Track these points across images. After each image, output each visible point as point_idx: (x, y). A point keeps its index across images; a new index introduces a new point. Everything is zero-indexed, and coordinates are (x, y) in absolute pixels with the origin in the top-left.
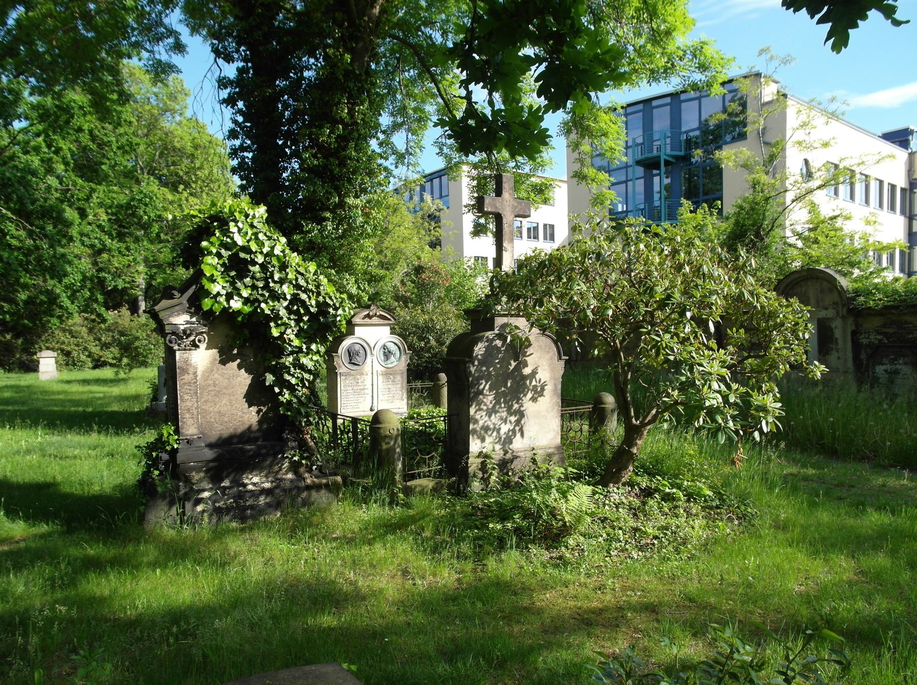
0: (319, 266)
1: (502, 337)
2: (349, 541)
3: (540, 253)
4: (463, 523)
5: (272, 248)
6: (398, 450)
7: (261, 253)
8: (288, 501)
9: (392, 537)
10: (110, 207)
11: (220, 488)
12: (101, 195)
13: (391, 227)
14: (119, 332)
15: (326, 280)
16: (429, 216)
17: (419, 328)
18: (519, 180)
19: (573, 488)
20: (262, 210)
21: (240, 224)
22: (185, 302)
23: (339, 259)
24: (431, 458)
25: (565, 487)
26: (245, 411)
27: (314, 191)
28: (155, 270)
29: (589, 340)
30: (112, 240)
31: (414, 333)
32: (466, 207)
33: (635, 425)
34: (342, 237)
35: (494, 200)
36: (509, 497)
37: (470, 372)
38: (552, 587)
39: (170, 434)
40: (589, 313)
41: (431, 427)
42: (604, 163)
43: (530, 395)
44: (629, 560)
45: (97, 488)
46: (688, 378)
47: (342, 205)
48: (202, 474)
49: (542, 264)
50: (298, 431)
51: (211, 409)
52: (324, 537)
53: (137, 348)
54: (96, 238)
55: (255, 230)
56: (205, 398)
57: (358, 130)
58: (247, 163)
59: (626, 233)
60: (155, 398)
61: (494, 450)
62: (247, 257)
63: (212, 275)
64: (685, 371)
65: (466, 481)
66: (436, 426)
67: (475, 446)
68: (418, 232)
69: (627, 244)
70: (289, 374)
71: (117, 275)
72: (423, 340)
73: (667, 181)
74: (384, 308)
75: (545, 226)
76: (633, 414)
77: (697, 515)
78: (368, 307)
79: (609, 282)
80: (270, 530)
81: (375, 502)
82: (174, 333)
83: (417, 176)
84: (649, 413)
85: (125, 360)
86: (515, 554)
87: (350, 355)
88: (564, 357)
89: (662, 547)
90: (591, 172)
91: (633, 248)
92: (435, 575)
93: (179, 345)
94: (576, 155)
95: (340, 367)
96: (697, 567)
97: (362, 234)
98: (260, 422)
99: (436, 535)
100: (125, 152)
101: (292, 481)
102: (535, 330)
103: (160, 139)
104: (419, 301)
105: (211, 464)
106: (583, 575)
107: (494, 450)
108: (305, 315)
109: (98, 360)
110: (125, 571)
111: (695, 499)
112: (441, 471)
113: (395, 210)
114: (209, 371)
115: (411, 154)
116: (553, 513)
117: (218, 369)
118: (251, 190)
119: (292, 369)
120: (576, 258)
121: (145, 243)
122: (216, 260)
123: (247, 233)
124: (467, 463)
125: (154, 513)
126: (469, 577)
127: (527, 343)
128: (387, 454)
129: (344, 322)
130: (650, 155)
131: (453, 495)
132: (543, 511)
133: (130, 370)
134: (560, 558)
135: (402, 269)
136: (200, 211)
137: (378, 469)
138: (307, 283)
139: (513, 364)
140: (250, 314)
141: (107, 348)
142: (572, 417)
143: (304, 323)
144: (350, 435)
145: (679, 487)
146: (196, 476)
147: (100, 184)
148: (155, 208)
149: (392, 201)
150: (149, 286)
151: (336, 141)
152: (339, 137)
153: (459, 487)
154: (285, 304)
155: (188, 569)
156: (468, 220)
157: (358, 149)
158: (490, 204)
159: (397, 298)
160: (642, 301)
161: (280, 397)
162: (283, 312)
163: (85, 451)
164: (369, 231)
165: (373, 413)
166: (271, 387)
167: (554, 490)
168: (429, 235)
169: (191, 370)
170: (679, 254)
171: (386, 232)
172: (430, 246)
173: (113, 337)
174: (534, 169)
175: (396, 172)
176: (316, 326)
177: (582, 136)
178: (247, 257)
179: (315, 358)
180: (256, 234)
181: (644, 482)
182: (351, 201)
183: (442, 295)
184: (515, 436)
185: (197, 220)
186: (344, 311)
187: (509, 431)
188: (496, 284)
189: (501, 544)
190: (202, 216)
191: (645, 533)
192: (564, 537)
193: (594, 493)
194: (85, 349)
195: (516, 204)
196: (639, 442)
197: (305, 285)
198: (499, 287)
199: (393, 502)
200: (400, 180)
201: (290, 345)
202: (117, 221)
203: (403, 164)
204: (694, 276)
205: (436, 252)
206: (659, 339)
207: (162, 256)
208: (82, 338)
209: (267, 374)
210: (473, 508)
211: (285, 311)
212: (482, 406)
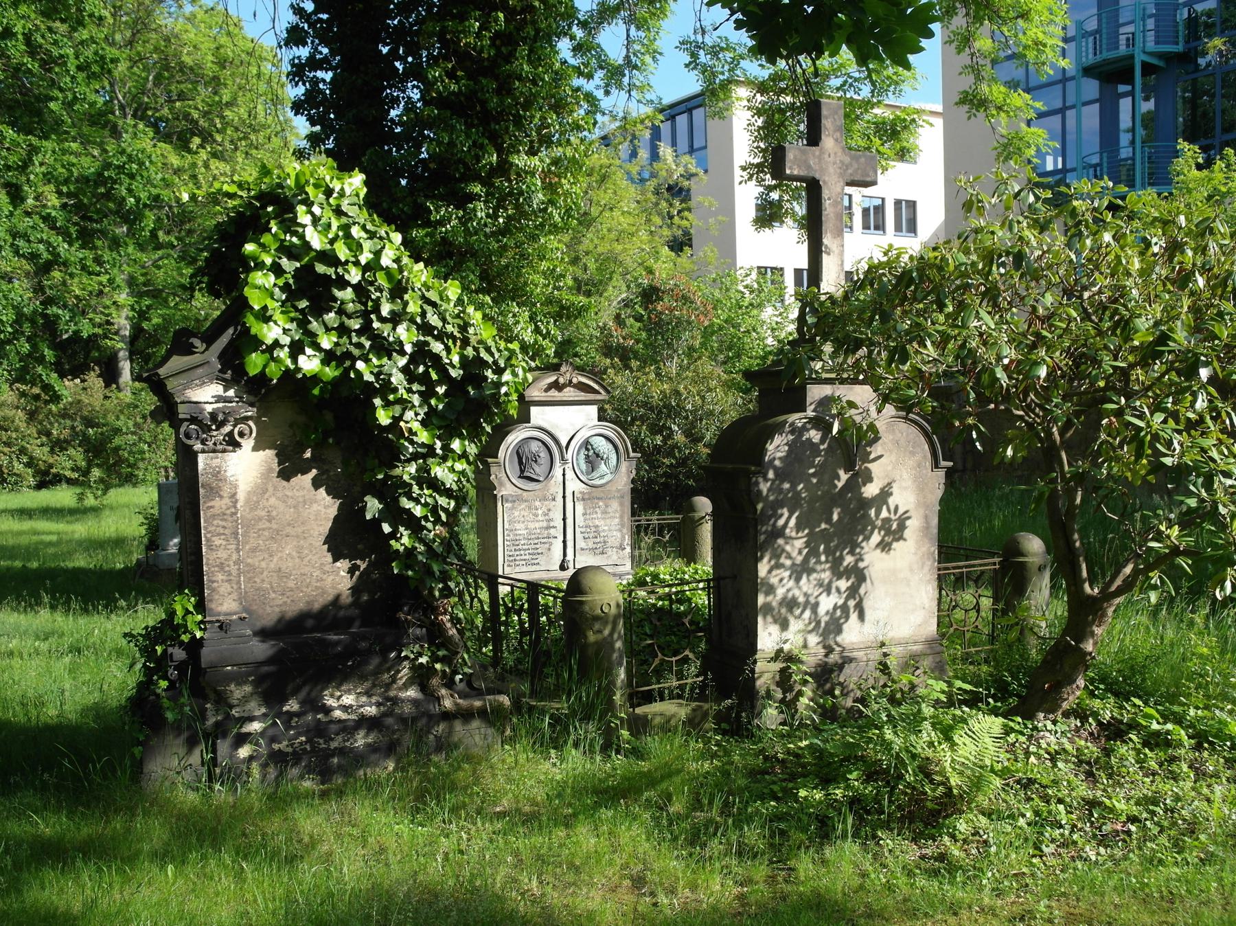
0: (465, 288)
1: (821, 423)
2: (529, 819)
3: (898, 256)
4: (747, 788)
5: (378, 254)
6: (618, 645)
7: (357, 263)
8: (408, 740)
9: (610, 813)
10: (66, 182)
11: (280, 714)
12: (49, 159)
13: (594, 211)
14: (84, 418)
15: (479, 315)
16: (670, 189)
17: (652, 409)
18: (852, 111)
19: (964, 721)
20: (356, 182)
21: (316, 210)
22: (214, 359)
23: (499, 275)
24: (686, 660)
25: (948, 720)
26: (327, 568)
27: (452, 144)
28: (147, 302)
29: (998, 425)
30: (70, 245)
31: (643, 419)
32: (744, 168)
33: (1090, 597)
34: (504, 231)
35: (803, 152)
36: (838, 737)
37: (760, 492)
38: (926, 914)
39: (188, 612)
40: (1000, 374)
41: (680, 602)
42: (1019, 74)
43: (876, 538)
44: (1079, 864)
45: (52, 712)
46: (1202, 501)
47: (504, 168)
48: (248, 689)
49: (905, 278)
50: (428, 608)
51: (263, 564)
52: (478, 813)
53: (117, 449)
54: (41, 241)
55: (344, 220)
56: (253, 543)
57: (534, 22)
58: (322, 92)
59: (1073, 213)
60: (154, 543)
61: (805, 646)
62: (331, 271)
63: (265, 308)
64: (1196, 485)
65: (753, 707)
66: (689, 600)
67: (768, 638)
68: (648, 221)
69: (1074, 235)
70: (410, 498)
71: (79, 311)
72: (660, 432)
73: (1148, 106)
74: (580, 369)
75: (898, 203)
76: (1085, 574)
77: (1216, 775)
78: (555, 368)
79: (1041, 311)
80: (375, 796)
81: (576, 745)
82: (193, 420)
83: (646, 110)
84: (1118, 572)
85: (96, 473)
86: (851, 848)
87: (520, 462)
88: (943, 463)
89: (1145, 839)
90: (996, 92)
91: (1088, 242)
92: (694, 887)
93: (203, 442)
94: (965, 58)
95: (501, 484)
96: (1220, 880)
97: (542, 225)
98: (355, 590)
99: (694, 809)
100: (92, 76)
101: (415, 702)
102: (889, 410)
103: (156, 49)
104: (652, 357)
105: (265, 669)
106: (987, 891)
107: (805, 646)
108: (439, 382)
109: (46, 473)
110: (109, 867)
111: (1211, 743)
112: (703, 687)
113: (604, 178)
114: (260, 491)
115: (635, 67)
116: (926, 770)
117: (275, 488)
118: (330, 144)
119: (415, 488)
120: (974, 264)
121: (130, 249)
122: (272, 278)
123: (329, 226)
124: (753, 671)
125: (159, 760)
126: (761, 891)
127: (871, 435)
128: (597, 653)
129: (515, 397)
130: (1112, 55)
131: (724, 733)
132: (905, 766)
133: (105, 492)
134: (942, 857)
135: (617, 293)
136: (240, 186)
137: (580, 682)
138: (444, 320)
139: (844, 476)
140: (336, 382)
141: (63, 449)
142: (959, 582)
143: (439, 399)
144: (525, 616)
145: (1179, 720)
146: (237, 692)
147: (46, 138)
148: (149, 181)
149: (598, 158)
150: (137, 331)
151: (493, 45)
152: (498, 35)
153: (738, 716)
154: (402, 361)
155: (226, 867)
156: (747, 196)
157: (535, 59)
158: (797, 159)
159: (608, 350)
160: (1106, 347)
161: (393, 542)
162: (397, 379)
163: (30, 642)
164: (557, 218)
165: (569, 573)
166: (376, 523)
167: (927, 725)
168: (670, 226)
169: (226, 491)
170: (1183, 252)
171: (586, 221)
172: (671, 248)
173: (73, 428)
174: (878, 90)
175: (606, 103)
176: (460, 405)
177: (978, 19)
178: (331, 271)
179: (459, 466)
180: (346, 228)
181: (1107, 710)
182: (521, 160)
183: (697, 344)
184: (847, 618)
185: (231, 203)
186: (515, 375)
187: (835, 608)
188: (810, 320)
189: (824, 830)
190: (244, 194)
191: (1112, 810)
192: (947, 816)
193: (1008, 731)
194: (23, 451)
195: (847, 160)
196: (1098, 631)
197: (439, 324)
198: (816, 325)
199: (609, 745)
200: (614, 118)
201: (412, 442)
202: (79, 208)
203: (620, 87)
204: (1214, 295)
205: (684, 260)
206: (1141, 424)
207: (161, 273)
208: (16, 430)
209: (368, 498)
210: (766, 758)
211: (401, 376)
212: (782, 560)
